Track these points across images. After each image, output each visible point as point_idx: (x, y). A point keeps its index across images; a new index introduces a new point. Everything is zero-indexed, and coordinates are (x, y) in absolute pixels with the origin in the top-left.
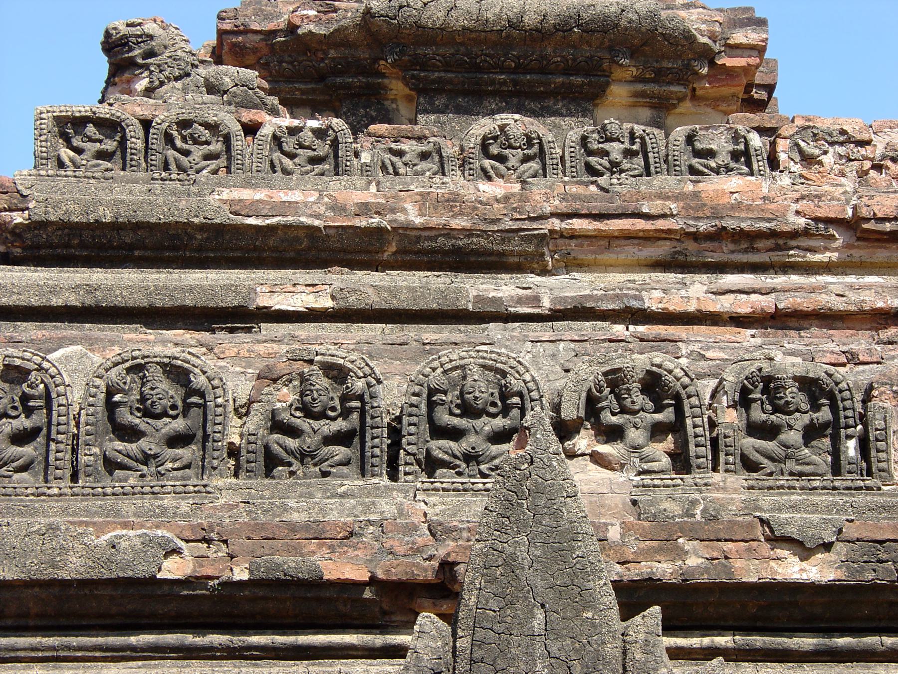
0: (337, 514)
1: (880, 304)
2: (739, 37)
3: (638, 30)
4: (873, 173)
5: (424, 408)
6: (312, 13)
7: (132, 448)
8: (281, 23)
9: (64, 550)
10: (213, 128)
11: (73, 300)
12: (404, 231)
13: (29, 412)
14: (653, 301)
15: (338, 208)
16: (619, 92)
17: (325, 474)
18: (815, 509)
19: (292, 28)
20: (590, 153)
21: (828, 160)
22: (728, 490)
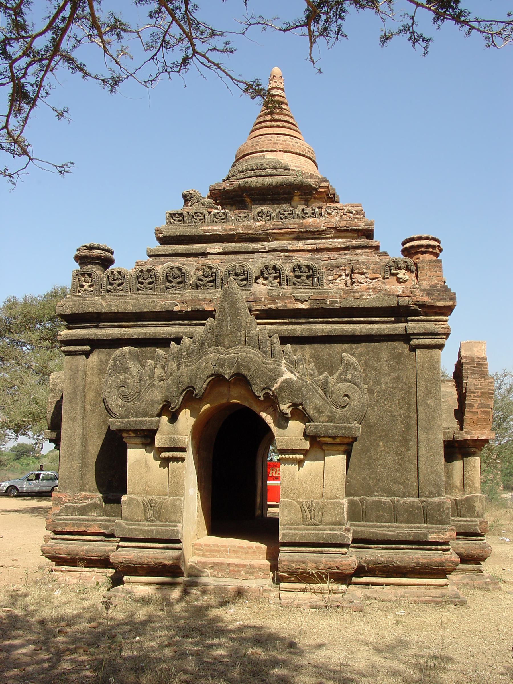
0: (208, 297)
1: (339, 246)
2: (322, 185)
3: (298, 185)
4: (343, 216)
5: (227, 275)
6: (228, 185)
7: (171, 284)
8: (222, 187)
9: (156, 306)
10: (202, 213)
11: (171, 253)
12: (239, 234)
13: (152, 278)
14: (290, 247)
15: (225, 230)
16: (296, 198)
17: (208, 289)
18: (305, 293)
19: (224, 188)
20: (281, 214)
21: (333, 213)
22: (288, 289)
